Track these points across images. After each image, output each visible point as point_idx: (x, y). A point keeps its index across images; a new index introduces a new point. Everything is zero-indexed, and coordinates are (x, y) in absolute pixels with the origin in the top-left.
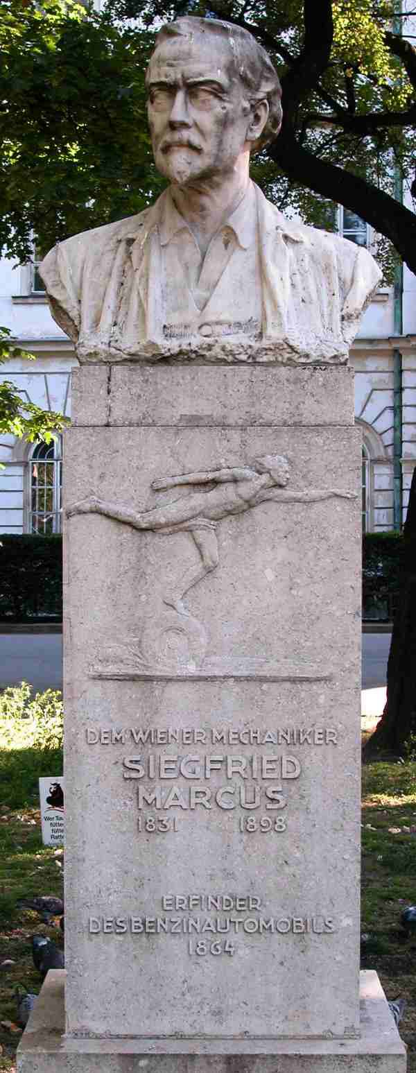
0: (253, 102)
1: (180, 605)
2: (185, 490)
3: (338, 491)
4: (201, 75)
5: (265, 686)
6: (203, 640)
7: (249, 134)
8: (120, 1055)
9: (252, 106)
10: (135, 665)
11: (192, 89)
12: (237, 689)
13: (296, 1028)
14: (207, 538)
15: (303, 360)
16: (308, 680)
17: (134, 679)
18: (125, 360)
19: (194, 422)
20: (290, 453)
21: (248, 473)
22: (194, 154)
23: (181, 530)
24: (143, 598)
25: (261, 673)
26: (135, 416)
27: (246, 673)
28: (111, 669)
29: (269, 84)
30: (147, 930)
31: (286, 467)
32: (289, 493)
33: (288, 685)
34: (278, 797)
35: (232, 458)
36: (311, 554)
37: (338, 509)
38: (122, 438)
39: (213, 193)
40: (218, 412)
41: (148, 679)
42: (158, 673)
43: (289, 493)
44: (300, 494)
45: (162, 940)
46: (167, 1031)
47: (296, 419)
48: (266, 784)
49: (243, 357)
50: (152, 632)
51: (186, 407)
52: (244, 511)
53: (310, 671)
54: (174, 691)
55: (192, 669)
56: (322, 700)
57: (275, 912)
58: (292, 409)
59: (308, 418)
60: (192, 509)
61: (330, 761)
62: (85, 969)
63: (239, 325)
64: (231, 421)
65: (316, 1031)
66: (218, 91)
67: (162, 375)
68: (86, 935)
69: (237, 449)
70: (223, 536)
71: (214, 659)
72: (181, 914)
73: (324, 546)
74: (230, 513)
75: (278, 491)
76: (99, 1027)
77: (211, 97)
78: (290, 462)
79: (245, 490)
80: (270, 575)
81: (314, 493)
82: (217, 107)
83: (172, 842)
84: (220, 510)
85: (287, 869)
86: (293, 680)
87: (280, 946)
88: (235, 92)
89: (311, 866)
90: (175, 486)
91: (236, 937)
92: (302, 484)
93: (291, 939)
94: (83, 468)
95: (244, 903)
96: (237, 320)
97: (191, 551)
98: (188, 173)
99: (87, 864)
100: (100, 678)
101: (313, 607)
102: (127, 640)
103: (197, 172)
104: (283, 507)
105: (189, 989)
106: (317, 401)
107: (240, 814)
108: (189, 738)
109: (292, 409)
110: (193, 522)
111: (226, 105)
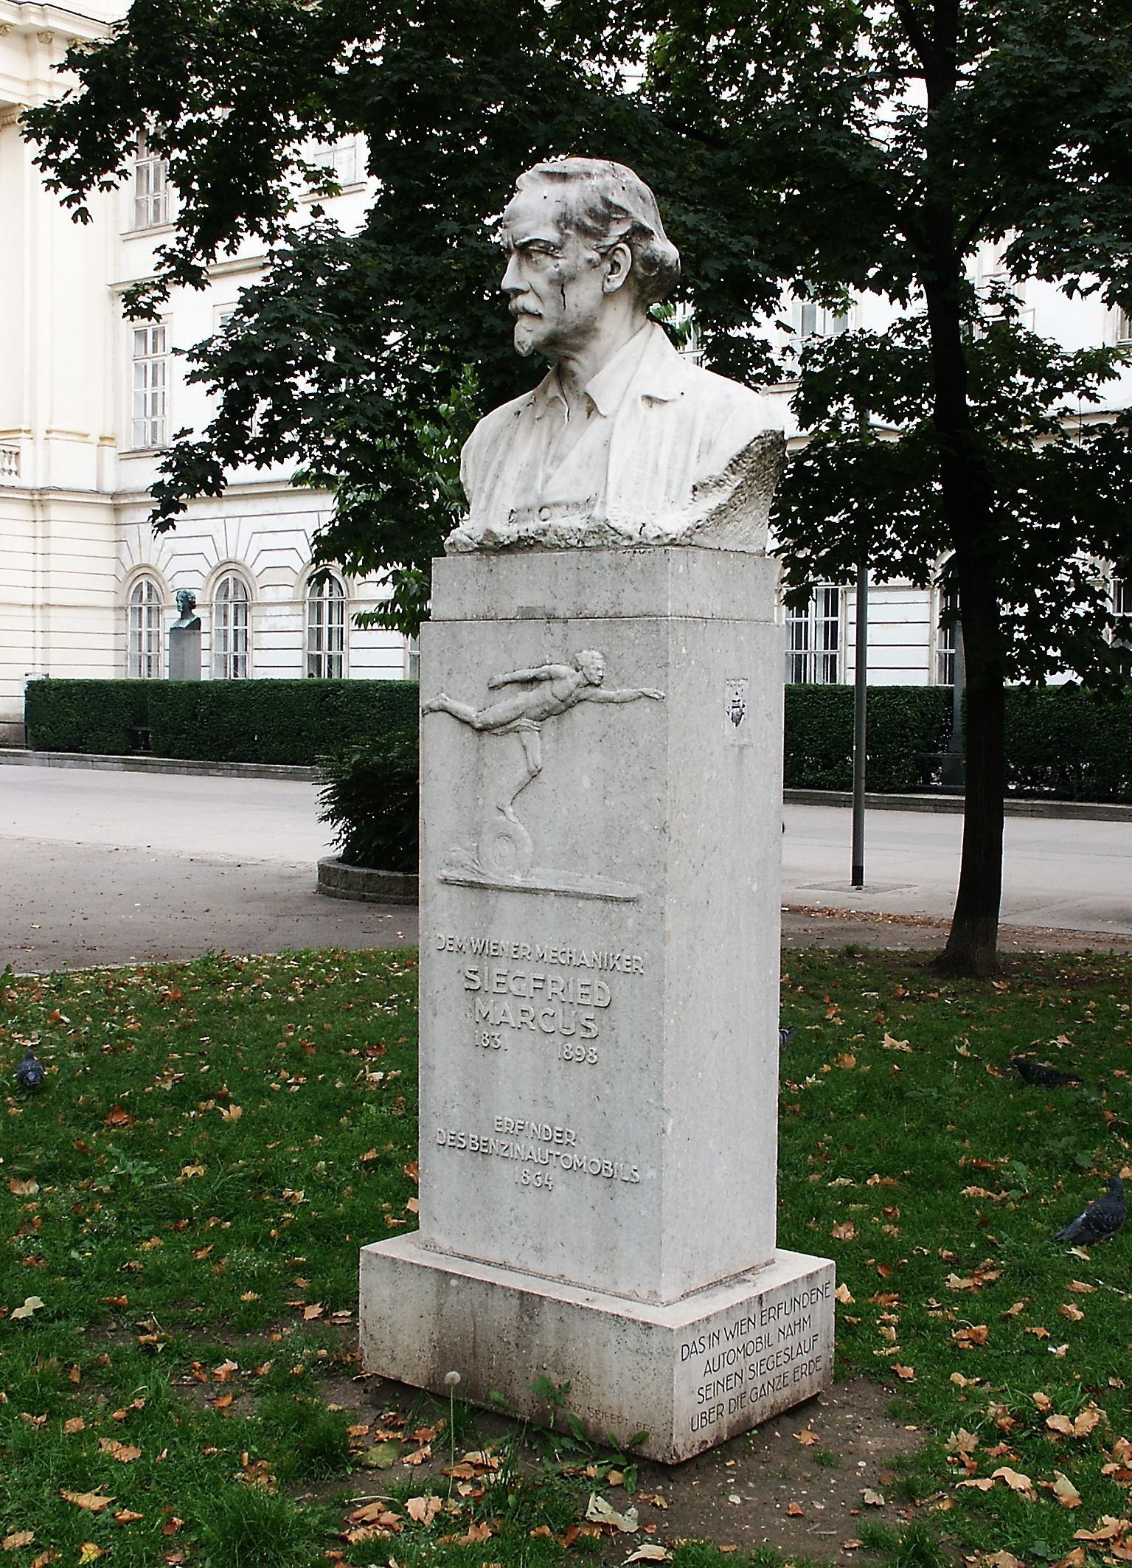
0: (602, 250)
1: (510, 810)
2: (515, 686)
3: (645, 690)
4: (527, 235)
5: (581, 903)
6: (528, 849)
7: (607, 286)
8: (437, 1270)
9: (603, 255)
10: (473, 871)
11: (525, 250)
12: (557, 905)
13: (600, 1280)
14: (531, 738)
15: (626, 543)
16: (617, 899)
17: (471, 885)
18: (476, 549)
19: (527, 615)
20: (606, 649)
21: (563, 669)
22: (537, 321)
23: (510, 730)
24: (480, 802)
25: (577, 889)
26: (481, 610)
27: (563, 887)
28: (454, 874)
29: (622, 224)
30: (481, 1151)
31: (600, 664)
32: (603, 692)
33: (600, 904)
34: (590, 1024)
35: (556, 653)
36: (622, 761)
37: (648, 710)
38: (464, 633)
39: (578, 356)
40: (549, 604)
41: (483, 887)
42: (489, 882)
43: (603, 692)
44: (612, 694)
45: (494, 1161)
46: (553, 1272)
47: (617, 609)
48: (581, 1010)
49: (574, 542)
50: (488, 837)
51: (524, 599)
52: (562, 712)
53: (619, 890)
54: (507, 901)
55: (517, 880)
56: (630, 923)
57: (584, 1153)
58: (613, 599)
59: (627, 609)
60: (516, 708)
61: (637, 991)
62: (434, 1180)
63: (577, 505)
64: (559, 613)
65: (624, 1290)
66: (549, 249)
67: (506, 564)
68: (435, 1147)
69: (559, 643)
70: (546, 739)
71: (538, 870)
72: (508, 1137)
73: (634, 751)
74: (550, 714)
75: (591, 690)
76: (444, 1243)
77: (542, 256)
78: (605, 658)
79: (560, 689)
80: (586, 782)
81: (626, 692)
82: (550, 266)
83: (504, 1060)
84: (539, 710)
85: (599, 1106)
86: (606, 899)
87: (593, 1189)
88: (569, 245)
89: (619, 1105)
90: (506, 683)
91: (554, 1173)
92: (615, 682)
93: (600, 1182)
94: (435, 664)
95: (558, 1139)
96: (575, 500)
97: (519, 753)
98: (529, 342)
99: (437, 1073)
100: (445, 881)
101: (623, 820)
102: (468, 844)
103: (541, 339)
104: (599, 708)
105: (516, 1218)
106: (636, 589)
107: (559, 1040)
108: (517, 955)
109: (613, 599)
110: (517, 723)
111: (560, 262)
